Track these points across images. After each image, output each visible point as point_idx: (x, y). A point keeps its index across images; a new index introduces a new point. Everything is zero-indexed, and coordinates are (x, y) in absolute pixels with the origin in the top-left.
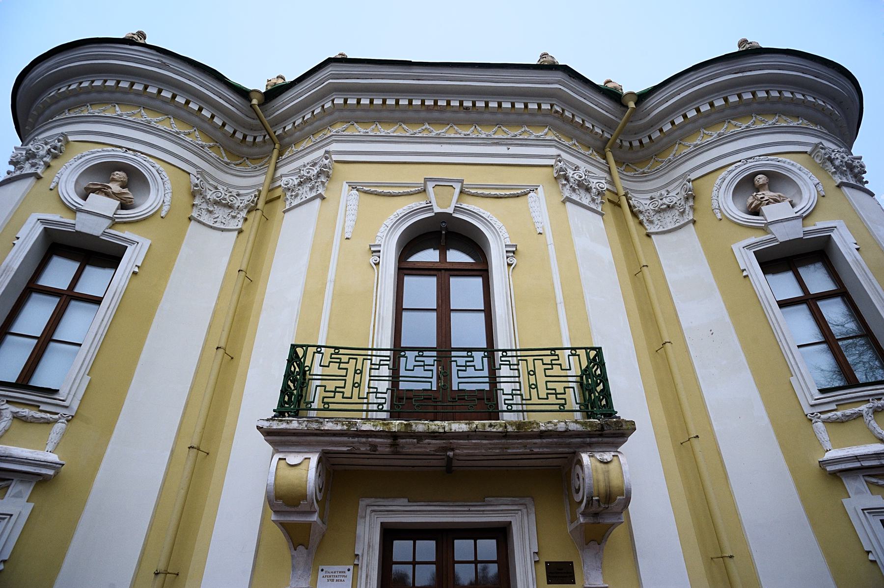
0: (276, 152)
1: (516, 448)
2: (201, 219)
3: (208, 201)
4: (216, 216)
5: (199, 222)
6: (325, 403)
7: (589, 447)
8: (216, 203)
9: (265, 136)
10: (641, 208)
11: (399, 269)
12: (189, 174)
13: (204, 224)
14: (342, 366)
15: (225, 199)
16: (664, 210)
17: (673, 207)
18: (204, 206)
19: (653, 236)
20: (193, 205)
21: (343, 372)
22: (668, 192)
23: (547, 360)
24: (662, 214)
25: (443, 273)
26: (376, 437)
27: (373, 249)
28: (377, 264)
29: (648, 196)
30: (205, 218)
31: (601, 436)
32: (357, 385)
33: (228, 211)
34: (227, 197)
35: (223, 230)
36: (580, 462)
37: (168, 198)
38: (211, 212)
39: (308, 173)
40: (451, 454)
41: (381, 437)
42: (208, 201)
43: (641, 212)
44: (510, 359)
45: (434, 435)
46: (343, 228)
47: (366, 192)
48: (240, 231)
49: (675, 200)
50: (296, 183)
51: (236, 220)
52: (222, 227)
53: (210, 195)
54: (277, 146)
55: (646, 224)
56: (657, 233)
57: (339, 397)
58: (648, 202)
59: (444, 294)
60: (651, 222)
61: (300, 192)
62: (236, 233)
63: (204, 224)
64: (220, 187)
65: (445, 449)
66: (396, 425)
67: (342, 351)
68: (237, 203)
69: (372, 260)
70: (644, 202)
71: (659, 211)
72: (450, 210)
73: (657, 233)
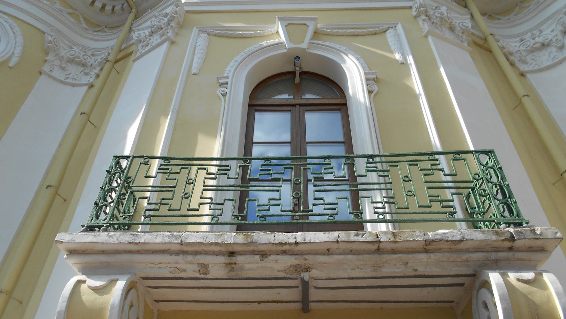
0: (132, 15)
1: (393, 266)
2: (53, 74)
3: (61, 58)
4: (68, 72)
5: (50, 76)
6: (146, 217)
7: (496, 265)
8: (71, 61)
9: (123, 5)
10: (511, 49)
11: (250, 105)
12: (44, 33)
13: (54, 79)
14: (172, 176)
15: (79, 58)
16: (539, 49)
17: (548, 45)
18: (57, 62)
19: (528, 76)
20: (46, 61)
21: (173, 183)
22: (541, 32)
23: (427, 165)
24: (535, 54)
25: (298, 110)
26: (207, 253)
27: (221, 81)
28: (224, 95)
29: (518, 39)
30: (57, 73)
31: (511, 249)
32: (187, 196)
33: (80, 68)
34: (81, 56)
35: (74, 85)
36: (487, 285)
37: (18, 51)
38: (63, 69)
39: (159, 22)
40: (306, 276)
41: (214, 253)
42: (61, 58)
43: (511, 54)
44: (379, 165)
45: (284, 250)
46: (191, 66)
47: (216, 35)
48: (91, 86)
49: (550, 37)
50: (147, 34)
51: (89, 77)
52: (74, 82)
53: (64, 52)
54: (134, 10)
55: (518, 64)
56: (532, 72)
57: (164, 210)
58: (518, 44)
59: (298, 129)
60: (525, 62)
61: (151, 41)
62: (86, 88)
63: (54, 79)
64: (74, 47)
65: (298, 269)
66: (231, 237)
67: (173, 162)
68: (91, 61)
69: (219, 91)
70: (513, 45)
71: (532, 50)
72: (304, 45)
73: (532, 72)
